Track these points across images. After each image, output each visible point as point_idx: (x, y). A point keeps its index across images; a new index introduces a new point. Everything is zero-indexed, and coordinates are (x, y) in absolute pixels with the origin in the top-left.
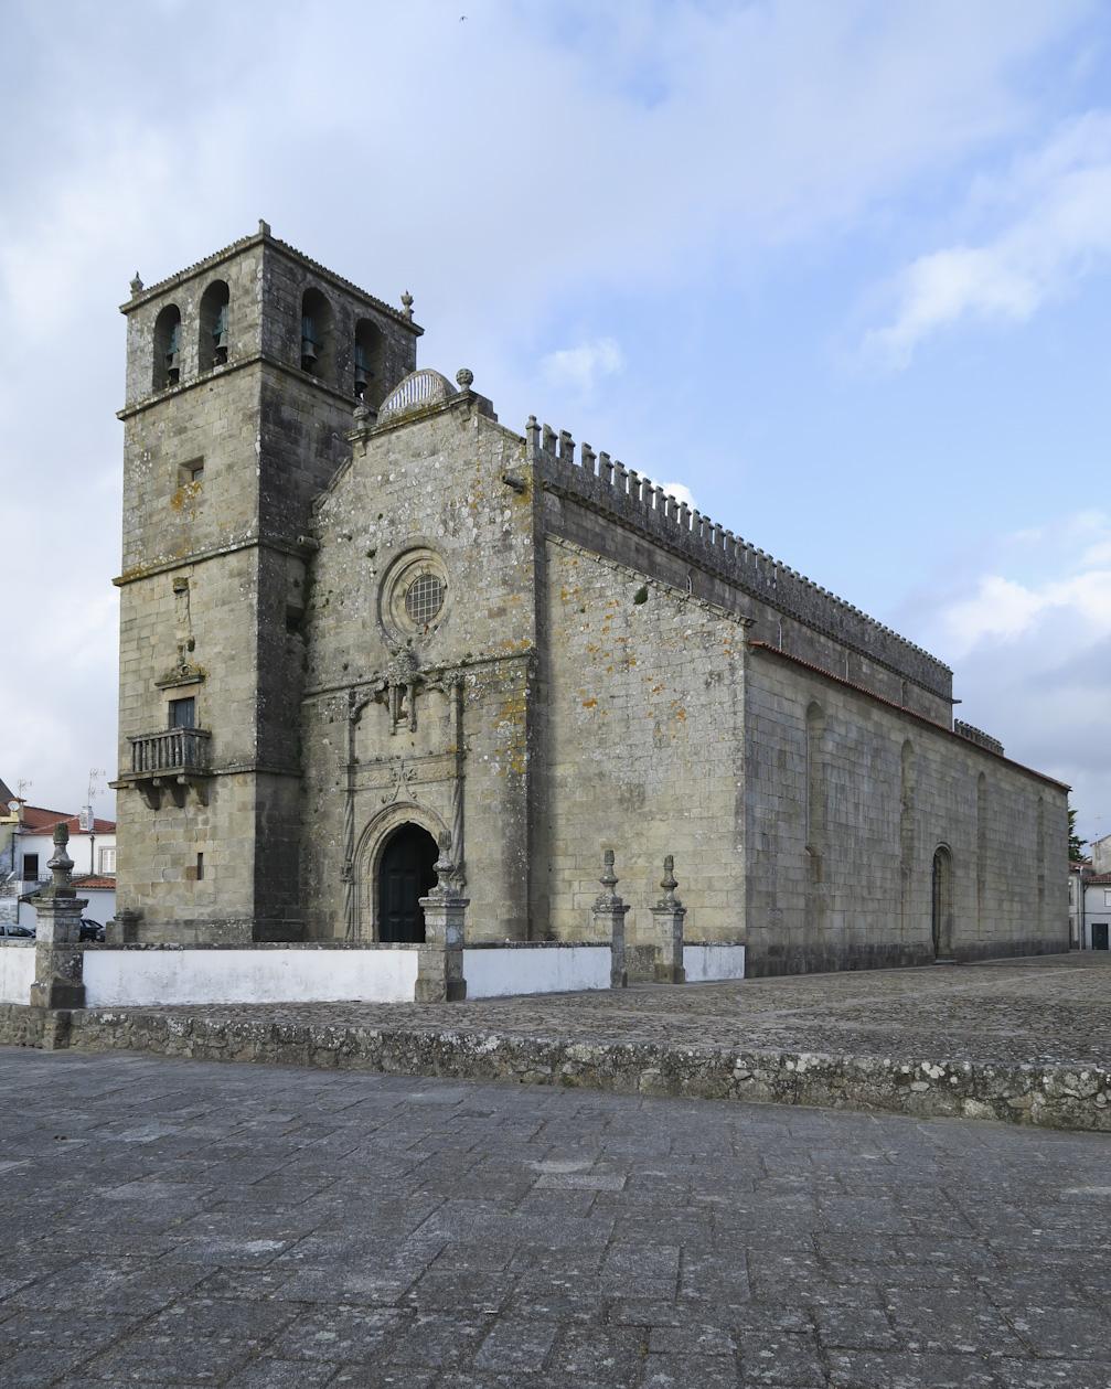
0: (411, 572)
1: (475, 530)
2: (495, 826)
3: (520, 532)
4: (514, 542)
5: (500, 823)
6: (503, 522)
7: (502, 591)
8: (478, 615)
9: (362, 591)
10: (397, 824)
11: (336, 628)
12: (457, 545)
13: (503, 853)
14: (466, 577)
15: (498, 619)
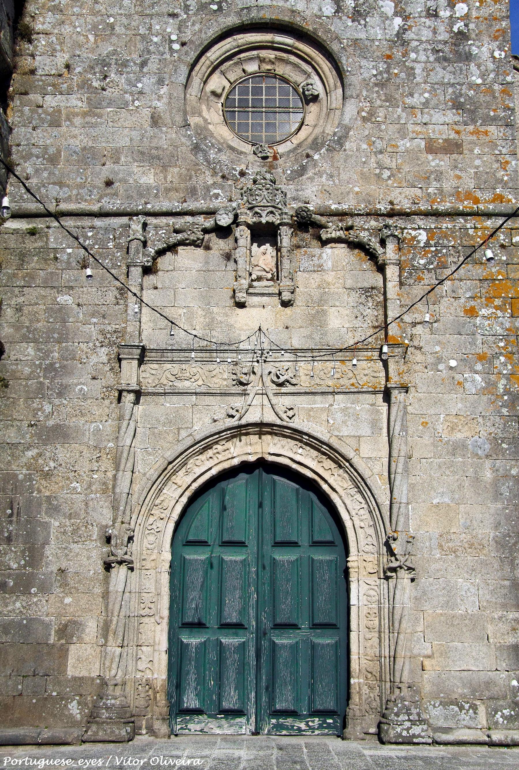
0: (241, 62)
1: (398, 21)
2: (477, 480)
3: (486, 39)
4: (475, 50)
5: (488, 475)
6: (452, 20)
7: (451, 116)
8: (404, 144)
9: (153, 66)
10: (236, 462)
11: (85, 115)
12: (362, 35)
13: (497, 526)
14: (381, 85)
15: (446, 158)
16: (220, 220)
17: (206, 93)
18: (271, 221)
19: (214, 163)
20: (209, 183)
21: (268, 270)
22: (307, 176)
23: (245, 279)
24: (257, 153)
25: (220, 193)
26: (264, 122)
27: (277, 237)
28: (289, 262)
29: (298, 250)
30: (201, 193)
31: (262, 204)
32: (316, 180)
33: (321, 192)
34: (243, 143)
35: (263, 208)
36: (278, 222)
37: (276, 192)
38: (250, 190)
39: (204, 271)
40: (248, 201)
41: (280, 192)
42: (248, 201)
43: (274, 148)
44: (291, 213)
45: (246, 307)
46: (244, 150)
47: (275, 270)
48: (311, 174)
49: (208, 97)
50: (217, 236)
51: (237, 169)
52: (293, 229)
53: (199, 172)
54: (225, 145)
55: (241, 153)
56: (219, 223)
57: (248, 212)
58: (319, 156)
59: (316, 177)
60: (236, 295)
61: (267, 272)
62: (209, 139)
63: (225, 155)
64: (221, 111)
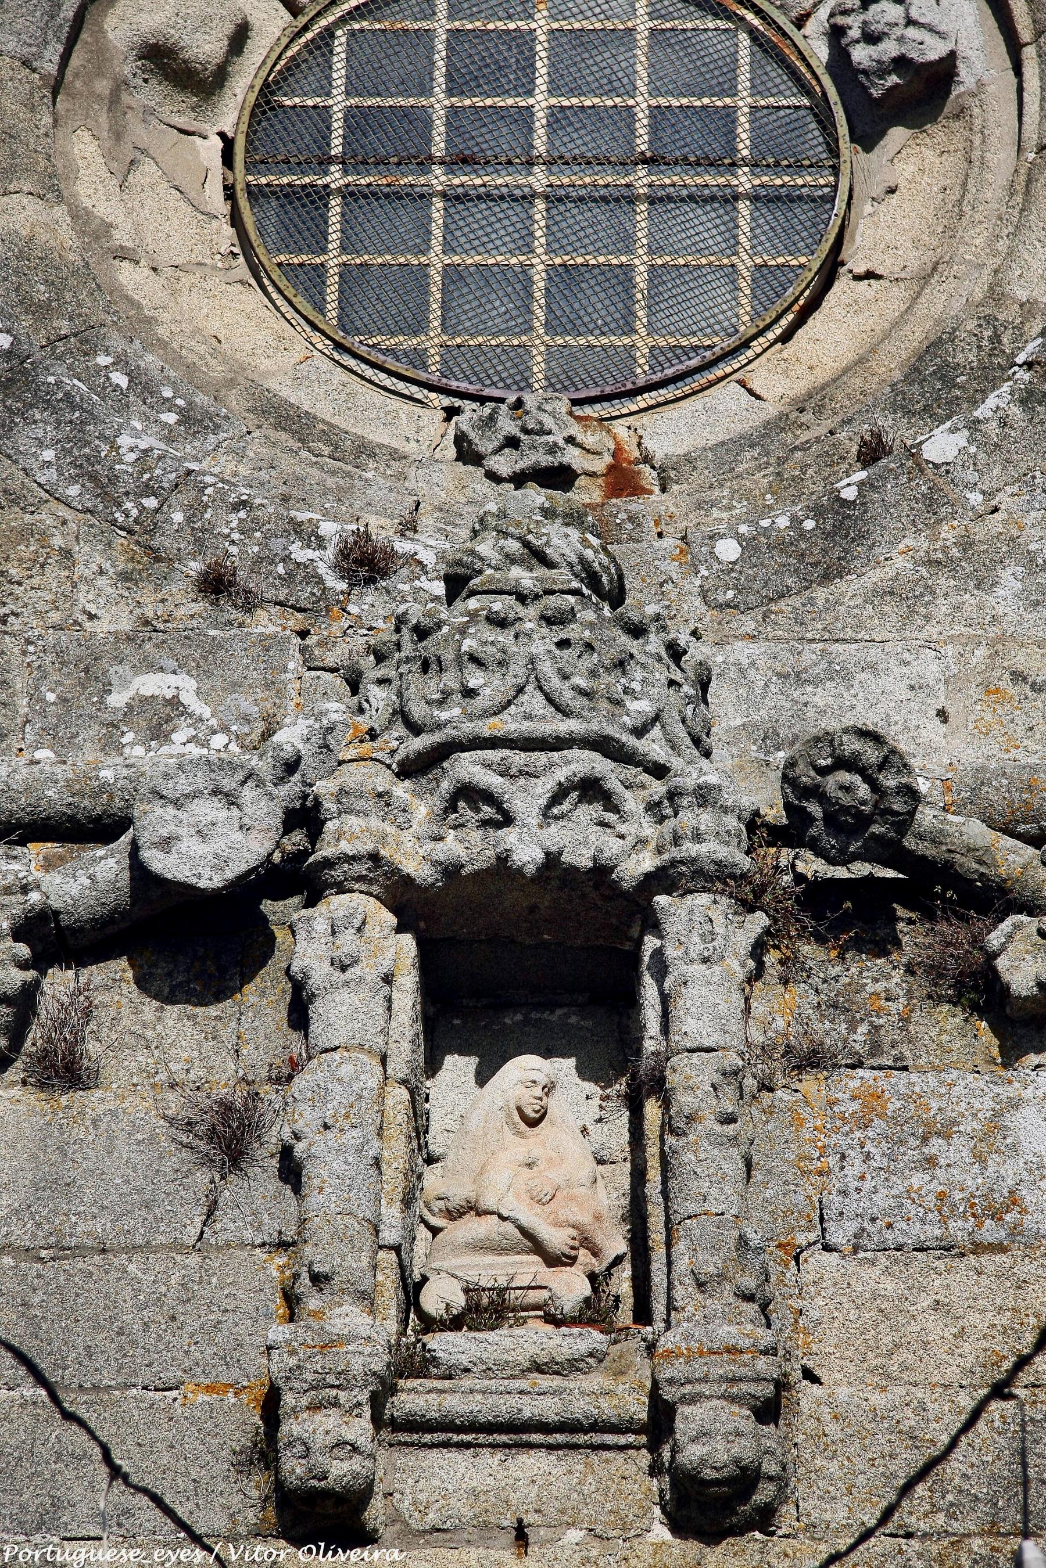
16: (166, 843)
17: (101, 53)
18: (583, 860)
19: (148, 490)
20: (102, 627)
21: (557, 1239)
22: (875, 576)
23: (367, 1298)
24: (485, 446)
25: (188, 699)
26: (539, 263)
27: (632, 1001)
28: (734, 1167)
29: (809, 1084)
30: (35, 696)
31: (509, 724)
32: (942, 608)
33: (989, 689)
34: (378, 398)
35: (517, 758)
36: (646, 862)
37: (633, 645)
38: (422, 633)
39: (29, 1253)
40: (401, 714)
41: (655, 643)
42: (401, 714)
43: (620, 428)
44: (747, 802)
45: (366, 1538)
46: (379, 436)
47: (617, 1244)
48: (901, 562)
49: (121, 85)
50: (143, 983)
51: (328, 528)
52: (760, 921)
53: (25, 551)
54: (235, 401)
55: (365, 450)
56: (157, 862)
57: (402, 790)
58: (961, 439)
59: (943, 582)
60: (290, 1428)
61: (554, 1260)
62: (116, 341)
63: (239, 455)
64: (214, 194)
